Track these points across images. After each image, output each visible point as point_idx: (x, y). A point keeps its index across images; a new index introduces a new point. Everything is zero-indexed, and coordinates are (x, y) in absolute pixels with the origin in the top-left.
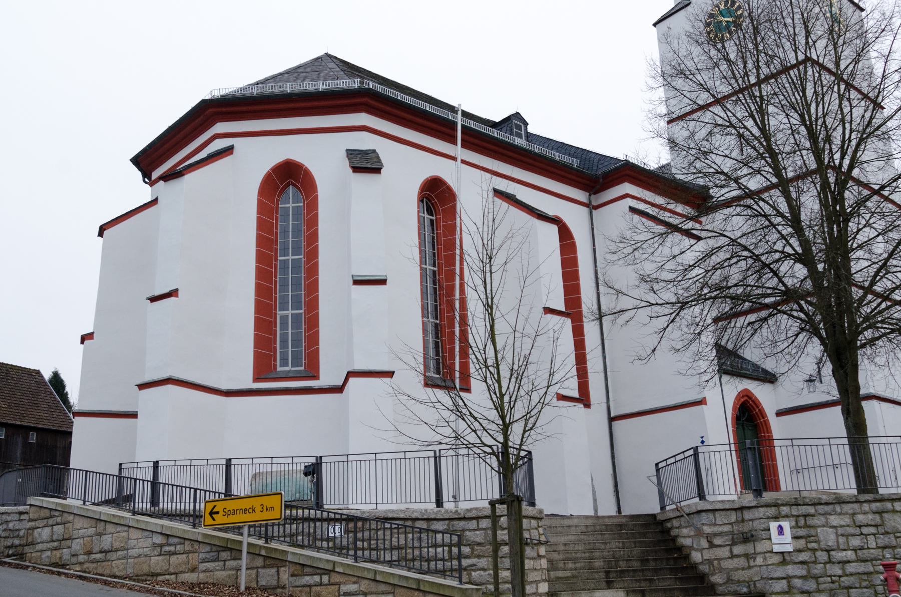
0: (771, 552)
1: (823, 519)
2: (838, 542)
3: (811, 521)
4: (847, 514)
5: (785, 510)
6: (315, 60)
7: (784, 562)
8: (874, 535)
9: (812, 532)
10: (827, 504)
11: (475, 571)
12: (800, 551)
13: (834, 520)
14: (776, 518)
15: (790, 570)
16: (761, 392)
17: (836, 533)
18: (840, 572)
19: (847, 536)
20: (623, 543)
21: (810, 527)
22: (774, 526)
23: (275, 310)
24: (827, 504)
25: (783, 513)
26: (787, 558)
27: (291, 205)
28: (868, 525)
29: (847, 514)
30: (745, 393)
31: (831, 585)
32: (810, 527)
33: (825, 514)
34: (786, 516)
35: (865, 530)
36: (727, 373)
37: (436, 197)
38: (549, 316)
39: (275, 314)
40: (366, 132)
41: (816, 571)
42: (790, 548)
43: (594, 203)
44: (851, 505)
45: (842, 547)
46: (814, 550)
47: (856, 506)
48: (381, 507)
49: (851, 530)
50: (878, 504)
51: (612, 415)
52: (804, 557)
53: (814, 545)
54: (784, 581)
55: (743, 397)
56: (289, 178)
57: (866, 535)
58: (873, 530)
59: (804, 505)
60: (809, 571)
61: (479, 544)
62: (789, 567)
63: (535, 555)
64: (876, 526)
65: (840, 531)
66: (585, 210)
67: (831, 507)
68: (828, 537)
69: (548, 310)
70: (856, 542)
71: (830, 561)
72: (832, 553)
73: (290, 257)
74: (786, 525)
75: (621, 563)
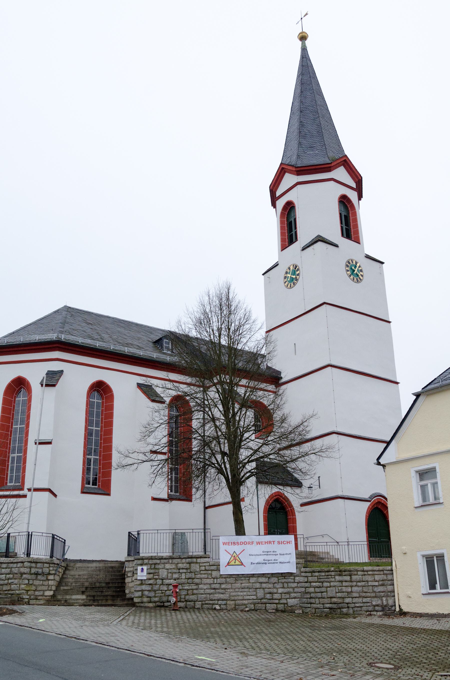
0: (137, 579)
1: (163, 565)
2: (168, 576)
3: (157, 566)
4: (174, 563)
5: (146, 561)
6: (55, 312)
7: (142, 584)
9: (157, 571)
10: (165, 559)
11: (13, 585)
12: (150, 579)
13: (168, 566)
14: (141, 565)
15: (144, 587)
16: (289, 493)
18: (166, 589)
19: (172, 573)
20: (106, 575)
21: (156, 569)
22: (139, 568)
24: (165, 559)
25: (145, 563)
26: (143, 582)
27: (21, 399)
28: (183, 569)
29: (174, 563)
30: (277, 494)
31: (161, 594)
32: (156, 569)
33: (164, 563)
34: (146, 564)
35: (181, 571)
37: (100, 389)
39: (9, 456)
40: (53, 361)
41: (155, 588)
42: (145, 578)
44: (177, 560)
45: (169, 578)
46: (156, 579)
47: (179, 560)
48: (159, 555)
49: (175, 571)
50: (190, 560)
51: (207, 506)
52: (151, 582)
53: (157, 577)
54: (140, 592)
55: (275, 496)
56: (19, 385)
57: (181, 573)
58: (185, 571)
59: (155, 559)
60: (152, 588)
61: (16, 574)
62: (144, 586)
63: (45, 579)
64: (187, 569)
65: (170, 571)
67: (167, 560)
68: (163, 573)
70: (176, 576)
71: (162, 584)
72: (164, 580)
73: (19, 426)
75: (97, 584)
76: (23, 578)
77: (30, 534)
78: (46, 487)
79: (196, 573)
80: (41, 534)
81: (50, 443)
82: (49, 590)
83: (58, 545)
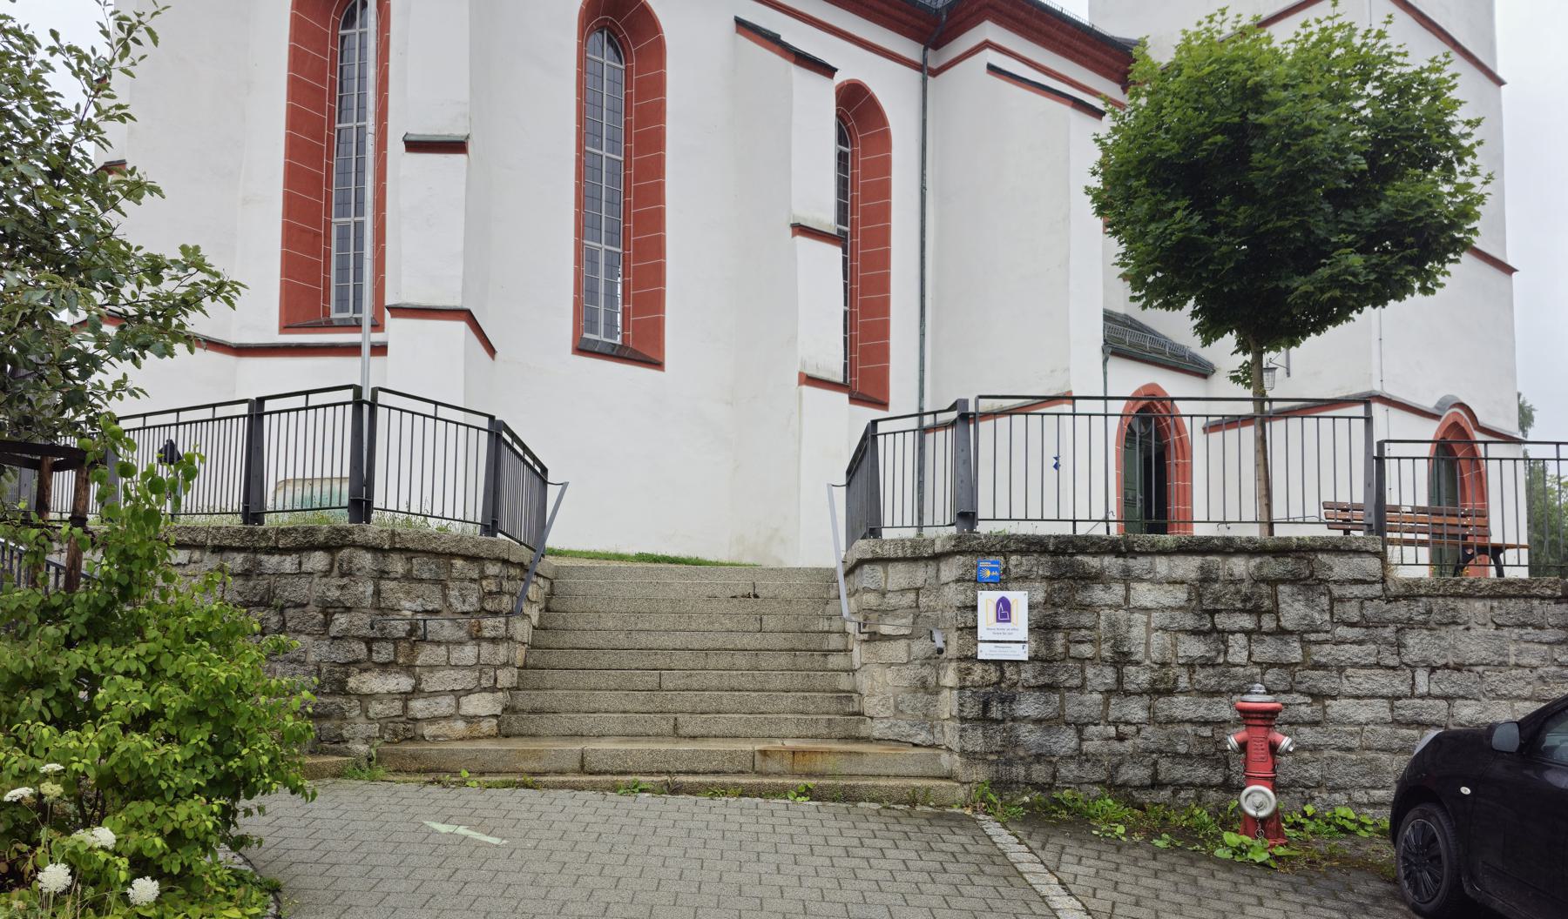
8: (1248, 633)
14: (1003, 581)
17: (1148, 624)
22: (987, 600)
23: (328, 213)
34: (1024, 579)
36: (1118, 353)
38: (802, 241)
39: (328, 224)
43: (932, 64)
66: (916, 76)
69: (801, 230)
74: (1019, 600)
76: (333, 631)
77: (367, 396)
78: (456, 303)
79: (1313, 637)
80: (429, 409)
81: (457, 146)
82: (485, 690)
83: (515, 477)
